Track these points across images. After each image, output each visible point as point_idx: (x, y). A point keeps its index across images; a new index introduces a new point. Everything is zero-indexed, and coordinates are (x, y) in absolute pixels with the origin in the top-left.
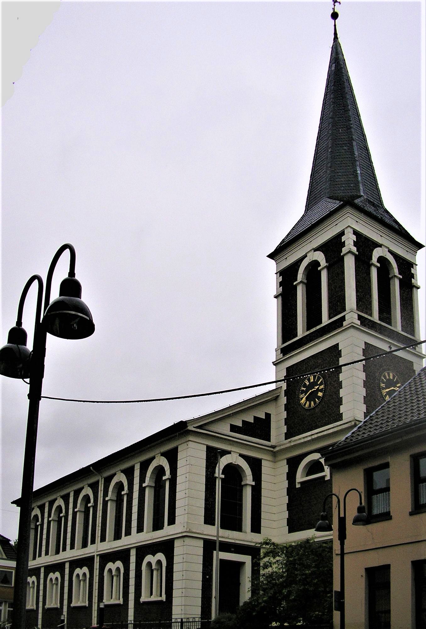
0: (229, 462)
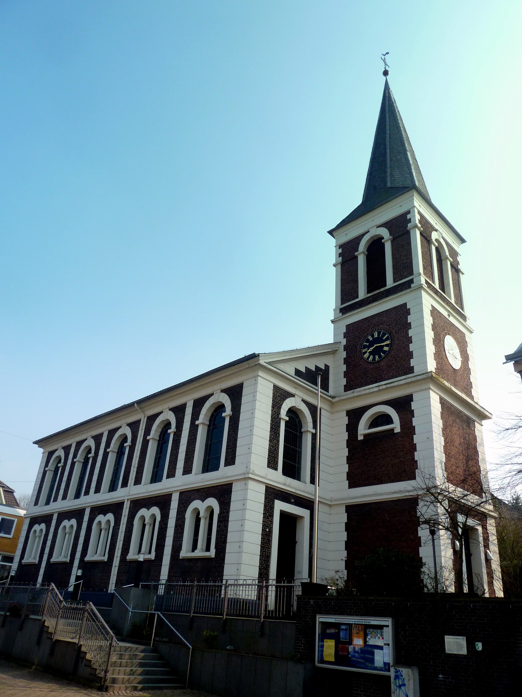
0: (293, 405)
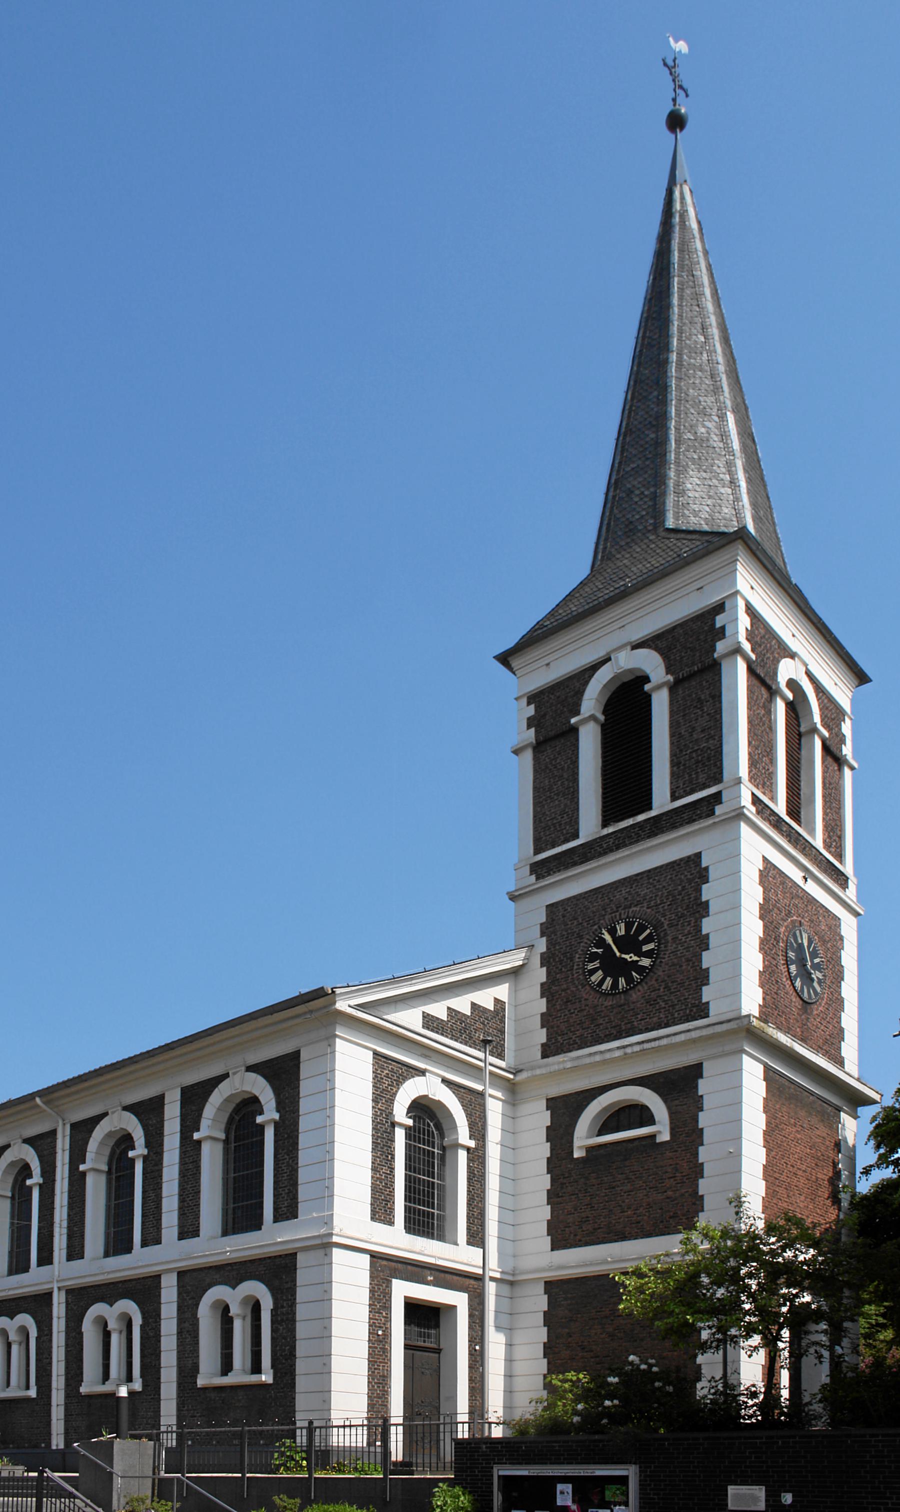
0: (421, 1094)
